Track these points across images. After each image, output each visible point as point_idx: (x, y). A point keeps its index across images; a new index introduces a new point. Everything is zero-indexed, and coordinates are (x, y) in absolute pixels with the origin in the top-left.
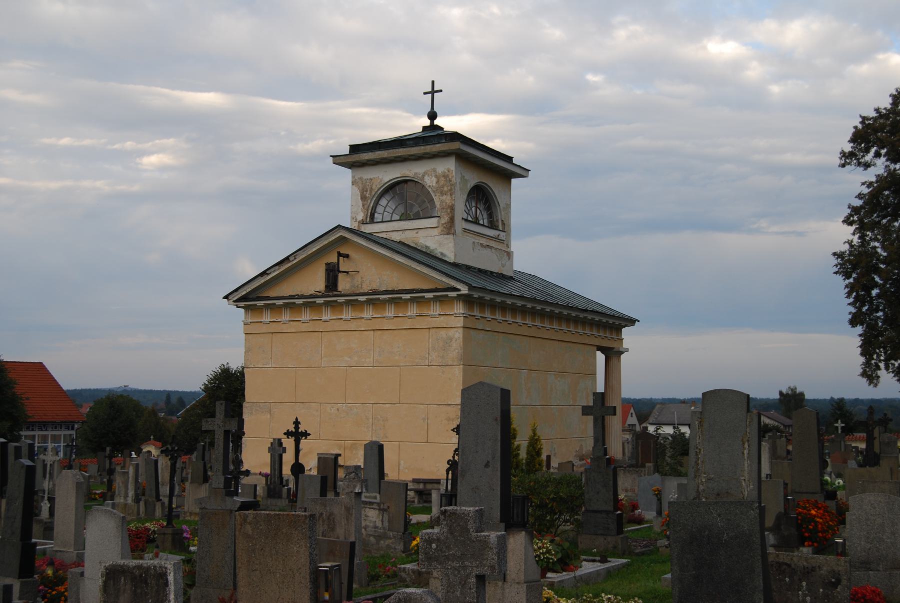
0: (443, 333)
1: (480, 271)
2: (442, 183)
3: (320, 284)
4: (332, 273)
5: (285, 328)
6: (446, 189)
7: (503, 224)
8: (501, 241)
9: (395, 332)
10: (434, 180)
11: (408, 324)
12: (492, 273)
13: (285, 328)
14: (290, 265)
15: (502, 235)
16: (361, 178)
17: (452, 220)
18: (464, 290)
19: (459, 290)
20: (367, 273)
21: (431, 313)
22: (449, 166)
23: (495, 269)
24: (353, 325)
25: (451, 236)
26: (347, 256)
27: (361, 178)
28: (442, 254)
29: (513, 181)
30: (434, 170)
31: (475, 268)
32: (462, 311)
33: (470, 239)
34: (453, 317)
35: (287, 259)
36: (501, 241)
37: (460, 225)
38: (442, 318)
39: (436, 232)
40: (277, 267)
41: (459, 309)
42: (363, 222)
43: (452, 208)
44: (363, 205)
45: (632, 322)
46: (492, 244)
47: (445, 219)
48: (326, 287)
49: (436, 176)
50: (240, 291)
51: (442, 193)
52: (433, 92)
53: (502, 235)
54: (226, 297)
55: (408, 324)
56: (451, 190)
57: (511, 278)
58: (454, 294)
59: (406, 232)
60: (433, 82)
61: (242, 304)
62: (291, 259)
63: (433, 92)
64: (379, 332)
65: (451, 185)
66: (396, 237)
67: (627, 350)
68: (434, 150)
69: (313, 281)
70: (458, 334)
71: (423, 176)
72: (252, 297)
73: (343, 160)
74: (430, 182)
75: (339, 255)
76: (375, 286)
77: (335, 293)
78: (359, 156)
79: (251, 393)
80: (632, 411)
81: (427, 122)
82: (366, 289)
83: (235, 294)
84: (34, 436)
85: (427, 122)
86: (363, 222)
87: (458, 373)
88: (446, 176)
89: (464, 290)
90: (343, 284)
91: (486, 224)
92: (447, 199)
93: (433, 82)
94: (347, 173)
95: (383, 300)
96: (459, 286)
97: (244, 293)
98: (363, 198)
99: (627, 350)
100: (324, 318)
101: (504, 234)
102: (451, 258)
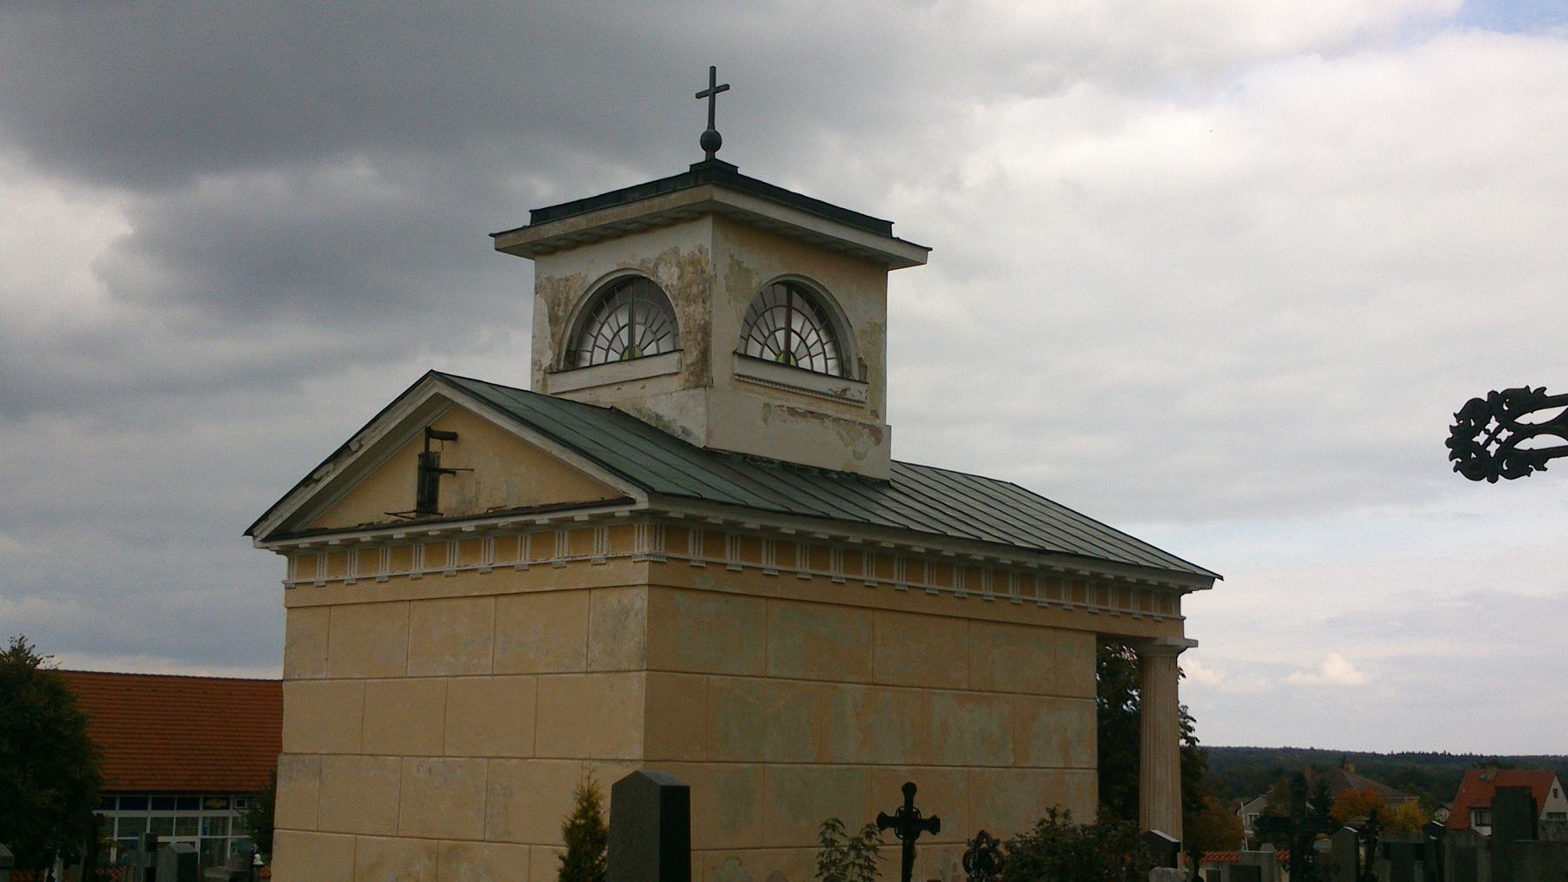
0: (613, 598)
1: (786, 467)
2: (689, 277)
3: (407, 501)
4: (430, 473)
5: (350, 595)
6: (694, 290)
7: (863, 366)
8: (856, 404)
9: (531, 598)
10: (675, 271)
11: (553, 580)
12: (823, 472)
13: (350, 595)
14: (352, 460)
15: (855, 391)
16: (549, 279)
17: (705, 355)
18: (643, 503)
19: (632, 502)
20: (490, 476)
21: (595, 556)
22: (699, 240)
23: (834, 463)
24: (460, 586)
25: (701, 390)
26: (453, 437)
27: (549, 279)
28: (684, 430)
29: (894, 276)
30: (676, 251)
31: (770, 461)
32: (646, 550)
33: (759, 398)
34: (630, 563)
35: (345, 449)
36: (856, 404)
37: (722, 367)
38: (612, 565)
39: (674, 384)
40: (330, 466)
41: (642, 545)
42: (552, 371)
43: (705, 330)
44: (553, 336)
45: (1205, 579)
46: (829, 409)
47: (692, 356)
48: (419, 504)
49: (680, 265)
50: (272, 518)
51: (689, 300)
52: (713, 91)
53: (855, 391)
54: (249, 532)
55: (553, 580)
56: (704, 291)
57: (886, 484)
58: (622, 511)
59: (625, 388)
60: (713, 70)
61: (277, 545)
62: (354, 446)
63: (713, 91)
64: (505, 599)
65: (705, 281)
66: (606, 398)
67: (1194, 644)
68: (667, 206)
69: (397, 493)
70: (639, 601)
71: (656, 266)
72: (295, 527)
73: (510, 241)
74: (667, 277)
75: (430, 434)
76: (498, 500)
77: (433, 517)
78: (547, 235)
79: (293, 736)
80: (1556, 784)
81: (701, 156)
82: (484, 506)
83: (265, 524)
84: (225, 819)
85: (701, 156)
86: (552, 371)
87: (636, 685)
88: (695, 262)
89: (643, 503)
90: (448, 498)
91: (834, 372)
92: (696, 311)
93: (713, 70)
94: (527, 266)
95: (504, 528)
96: (634, 493)
97: (279, 522)
98: (554, 320)
99: (1194, 644)
100: (414, 571)
101: (863, 388)
102: (699, 439)
